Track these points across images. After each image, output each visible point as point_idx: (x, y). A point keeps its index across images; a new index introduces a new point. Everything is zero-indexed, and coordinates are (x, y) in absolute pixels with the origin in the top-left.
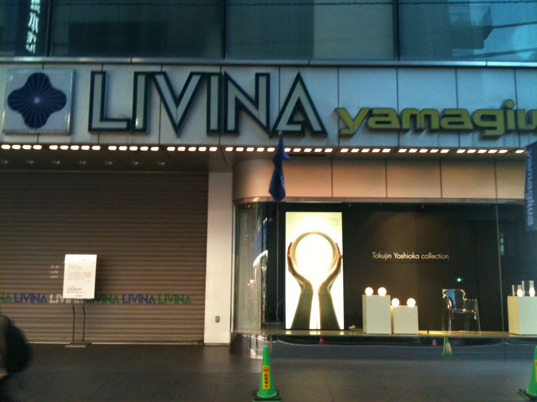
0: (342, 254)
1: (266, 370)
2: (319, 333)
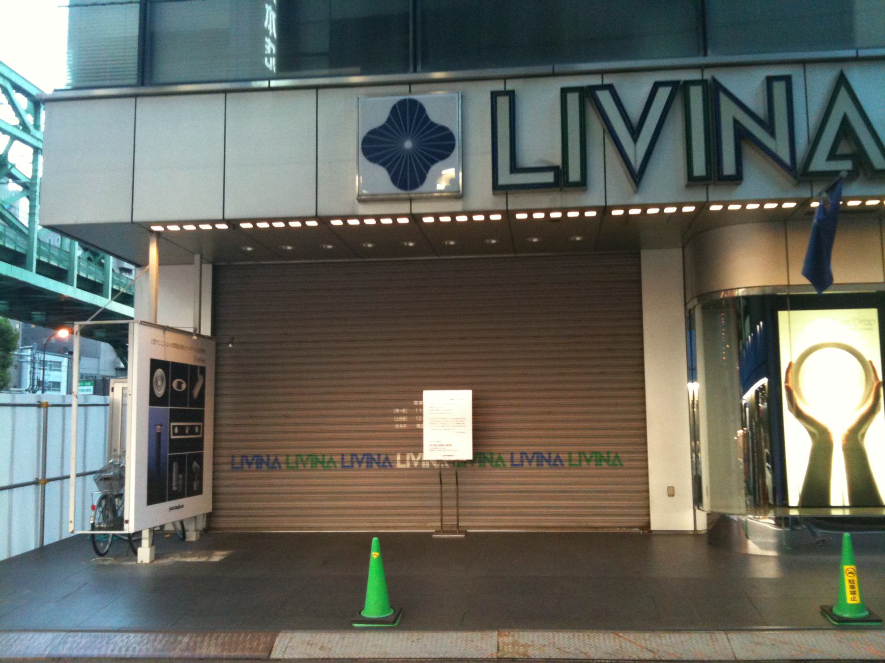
0: (880, 378)
1: (851, 573)
2: (847, 512)
